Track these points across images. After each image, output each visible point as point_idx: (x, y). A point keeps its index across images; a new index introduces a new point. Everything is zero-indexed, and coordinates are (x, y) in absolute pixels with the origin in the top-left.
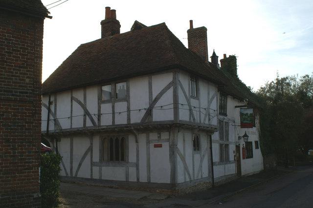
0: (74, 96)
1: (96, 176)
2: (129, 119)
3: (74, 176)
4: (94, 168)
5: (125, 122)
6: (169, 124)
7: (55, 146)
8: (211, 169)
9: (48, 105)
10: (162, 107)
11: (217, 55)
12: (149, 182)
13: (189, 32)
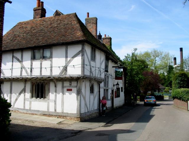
1: (27, 107)
11: (101, 35)
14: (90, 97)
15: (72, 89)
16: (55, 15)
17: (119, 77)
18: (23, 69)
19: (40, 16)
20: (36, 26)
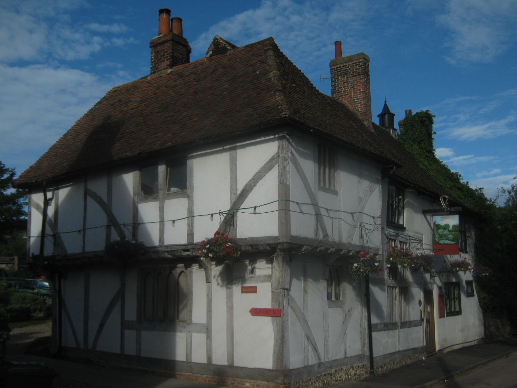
0: (379, 218)
1: (130, 350)
2: (191, 235)
3: (90, 347)
4: (127, 332)
5: (183, 240)
6: (269, 245)
7: (57, 287)
8: (367, 341)
9: (42, 205)
10: (255, 208)
11: (392, 111)
12: (231, 366)
13: (333, 64)
14: (122, 336)
15: (256, 288)
16: (211, 52)
17: (445, 244)
18: (113, 228)
19: (168, 62)
20: (155, 94)
